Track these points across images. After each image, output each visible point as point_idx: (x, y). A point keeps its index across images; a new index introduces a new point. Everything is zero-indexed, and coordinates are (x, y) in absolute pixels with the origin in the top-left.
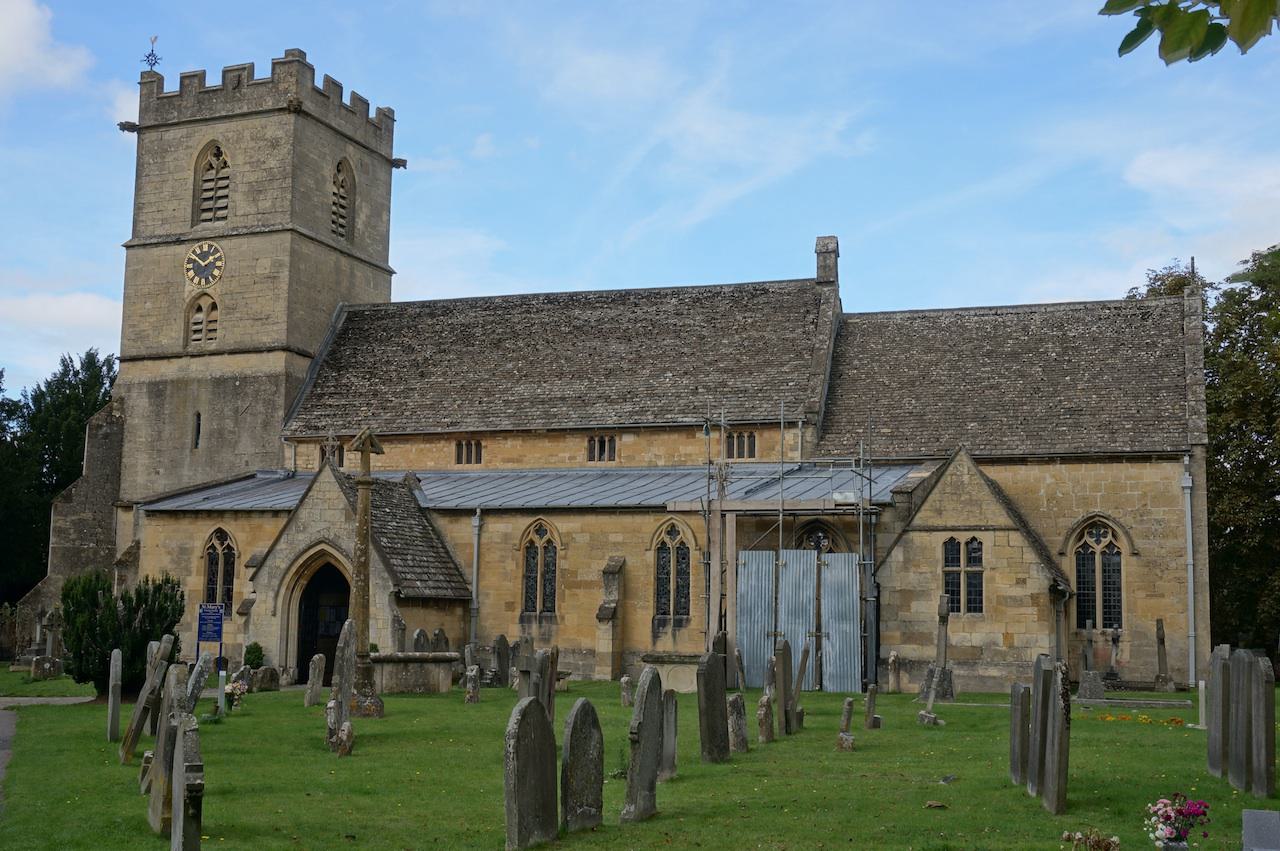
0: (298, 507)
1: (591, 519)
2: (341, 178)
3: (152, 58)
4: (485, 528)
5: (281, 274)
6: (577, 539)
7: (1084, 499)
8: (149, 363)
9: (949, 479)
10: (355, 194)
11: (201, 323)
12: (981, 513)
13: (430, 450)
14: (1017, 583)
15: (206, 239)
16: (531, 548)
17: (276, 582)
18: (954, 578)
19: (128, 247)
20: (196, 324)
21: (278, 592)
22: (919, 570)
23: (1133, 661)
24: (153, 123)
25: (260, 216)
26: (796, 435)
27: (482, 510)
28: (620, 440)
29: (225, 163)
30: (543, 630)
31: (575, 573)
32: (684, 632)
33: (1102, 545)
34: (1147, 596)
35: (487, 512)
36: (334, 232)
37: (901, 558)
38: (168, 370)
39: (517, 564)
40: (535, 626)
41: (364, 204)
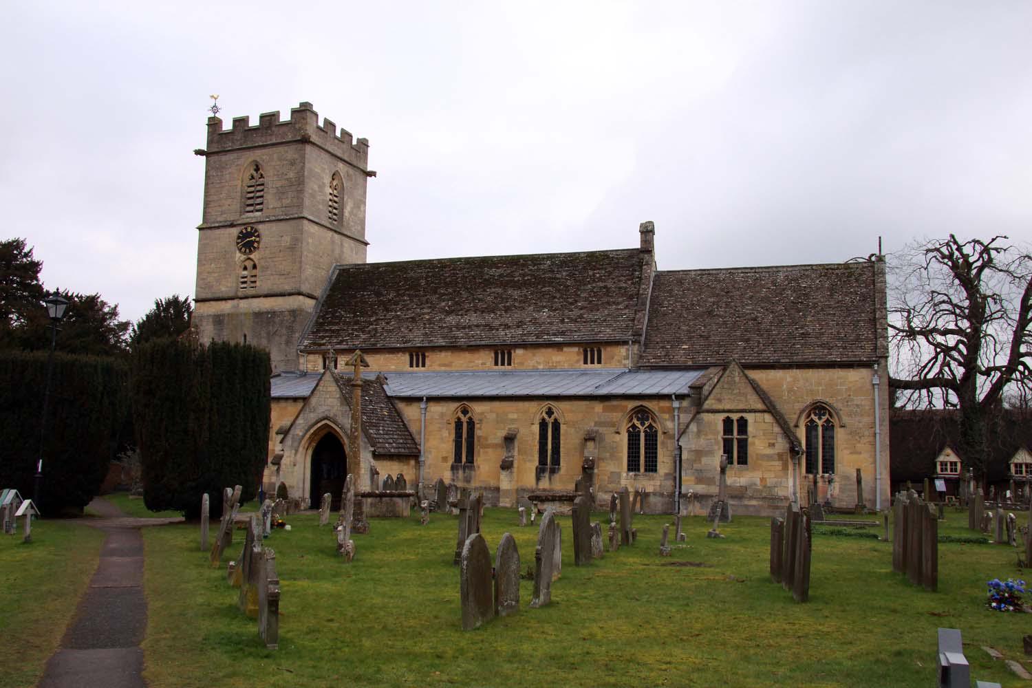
1: (497, 404)
3: (215, 109)
4: (428, 410)
6: (488, 417)
8: (213, 303)
11: (246, 277)
16: (459, 424)
17: (296, 444)
19: (200, 229)
20: (243, 278)
26: (628, 350)
28: (515, 352)
29: (262, 175)
30: (466, 475)
32: (556, 477)
33: (823, 420)
36: (330, 218)
38: (226, 307)
39: (449, 434)
40: (461, 472)
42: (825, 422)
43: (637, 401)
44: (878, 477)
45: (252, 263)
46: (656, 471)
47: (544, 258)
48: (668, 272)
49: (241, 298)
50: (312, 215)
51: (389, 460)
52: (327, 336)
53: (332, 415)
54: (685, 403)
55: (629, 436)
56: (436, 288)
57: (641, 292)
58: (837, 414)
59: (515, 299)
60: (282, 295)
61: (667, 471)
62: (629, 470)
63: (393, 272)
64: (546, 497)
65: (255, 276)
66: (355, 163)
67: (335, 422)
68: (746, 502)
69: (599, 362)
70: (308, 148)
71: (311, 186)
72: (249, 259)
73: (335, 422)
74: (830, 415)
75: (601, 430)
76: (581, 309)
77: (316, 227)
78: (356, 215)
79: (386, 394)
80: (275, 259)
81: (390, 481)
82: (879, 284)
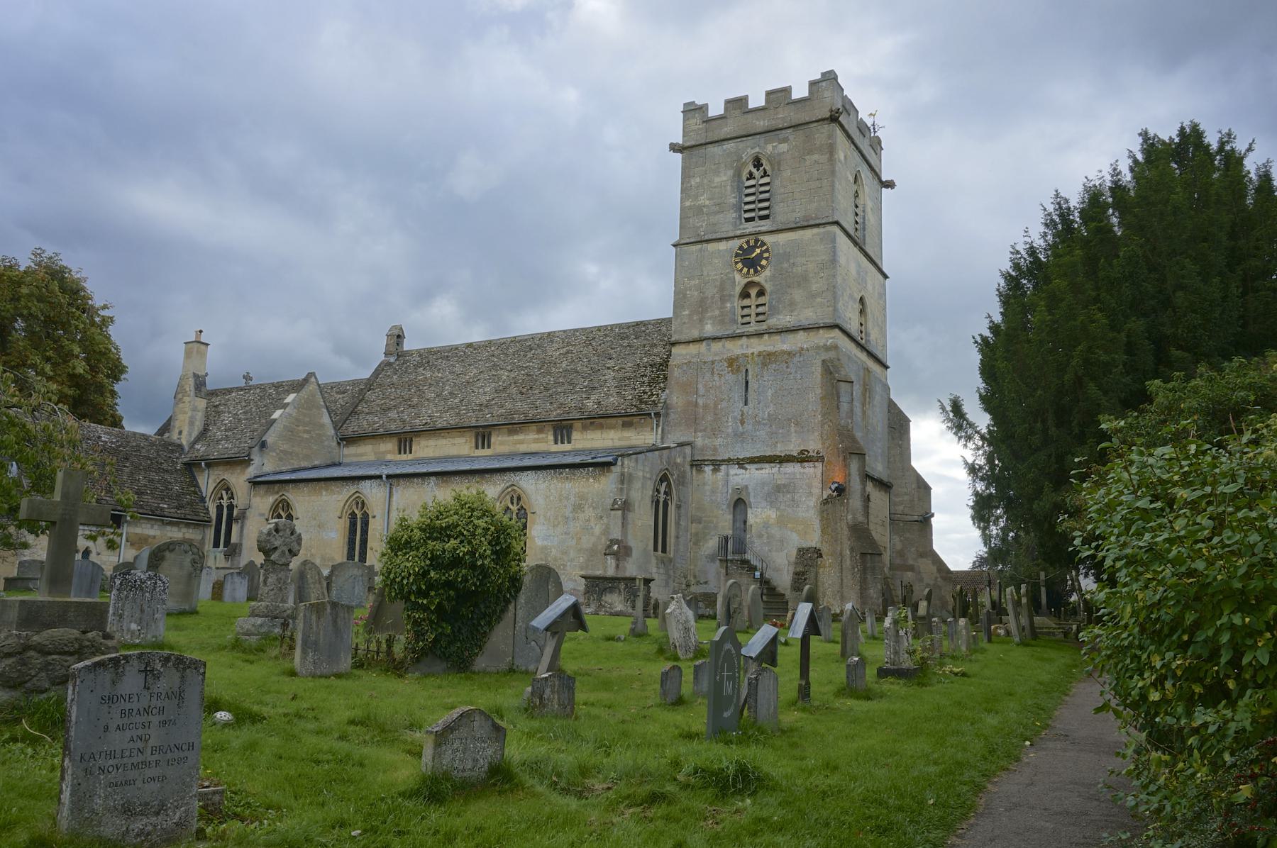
16: (353, 515)
21: (231, 569)
29: (765, 172)
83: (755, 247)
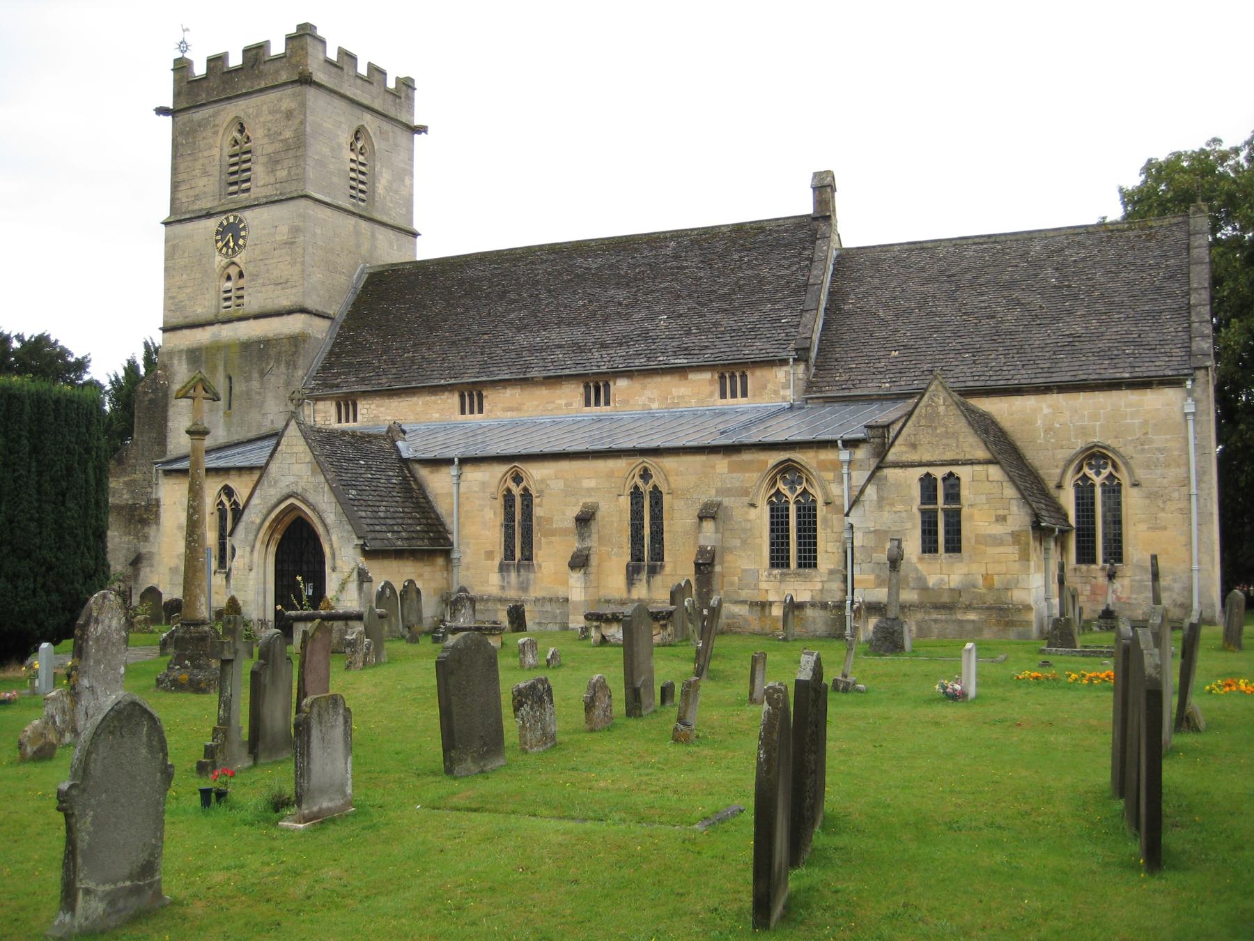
0: (267, 464)
1: (564, 465)
2: (359, 145)
3: (183, 46)
4: (463, 477)
5: (297, 240)
6: (552, 487)
7: (1083, 428)
8: (186, 332)
9: (924, 411)
10: (374, 161)
11: (230, 291)
12: (957, 446)
13: (435, 403)
14: (997, 520)
15: (232, 211)
16: (509, 499)
17: (251, 537)
18: (930, 517)
19: (166, 224)
20: (226, 292)
22: (894, 509)
23: (1134, 596)
24: (185, 105)
25: (278, 186)
26: (787, 373)
27: (459, 459)
28: (615, 384)
29: (248, 138)
30: (521, 579)
31: (550, 521)
32: (658, 579)
33: (1102, 476)
34: (1149, 528)
35: (464, 461)
36: (352, 196)
37: (875, 497)
38: (202, 337)
39: (495, 513)
40: (513, 575)
41: (384, 170)
42: (1107, 478)
43: (782, 453)
44: (1195, 566)
45: (238, 269)
46: (815, 565)
47: (666, 238)
48: (858, 248)
49: (224, 322)
50: (328, 194)
51: (395, 558)
52: (344, 373)
53: (299, 491)
54: (861, 453)
55: (772, 510)
56: (505, 293)
57: (811, 281)
58: (1126, 464)
59: (620, 304)
60: (278, 314)
61: (832, 567)
62: (773, 565)
63: (443, 272)
64: (614, 615)
65: (242, 288)
66: (392, 113)
67: (305, 501)
68: (960, 616)
69: (744, 394)
70: (311, 92)
71: (317, 149)
72: (234, 263)
73: (305, 501)
74: (1115, 466)
75: (727, 501)
76: (717, 313)
77: (328, 211)
78: (396, 192)
79: (401, 456)
80: (266, 262)
81: (388, 591)
82: (1196, 250)
83: (236, 243)
